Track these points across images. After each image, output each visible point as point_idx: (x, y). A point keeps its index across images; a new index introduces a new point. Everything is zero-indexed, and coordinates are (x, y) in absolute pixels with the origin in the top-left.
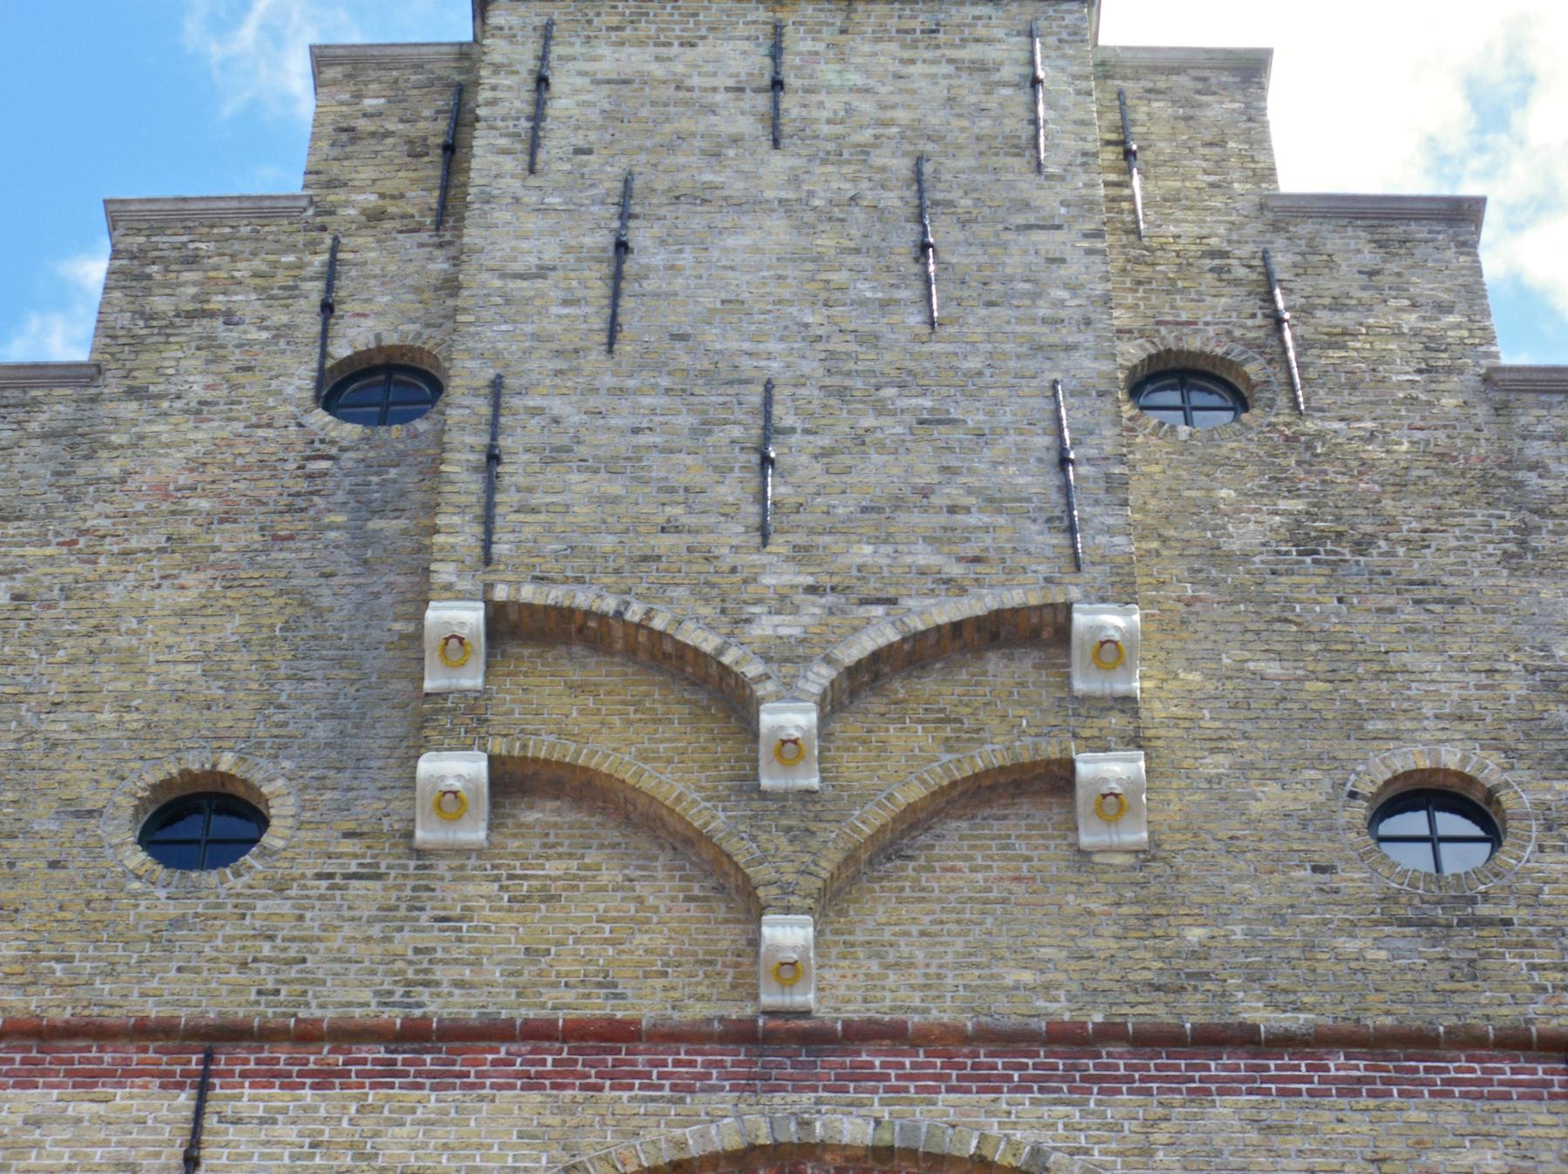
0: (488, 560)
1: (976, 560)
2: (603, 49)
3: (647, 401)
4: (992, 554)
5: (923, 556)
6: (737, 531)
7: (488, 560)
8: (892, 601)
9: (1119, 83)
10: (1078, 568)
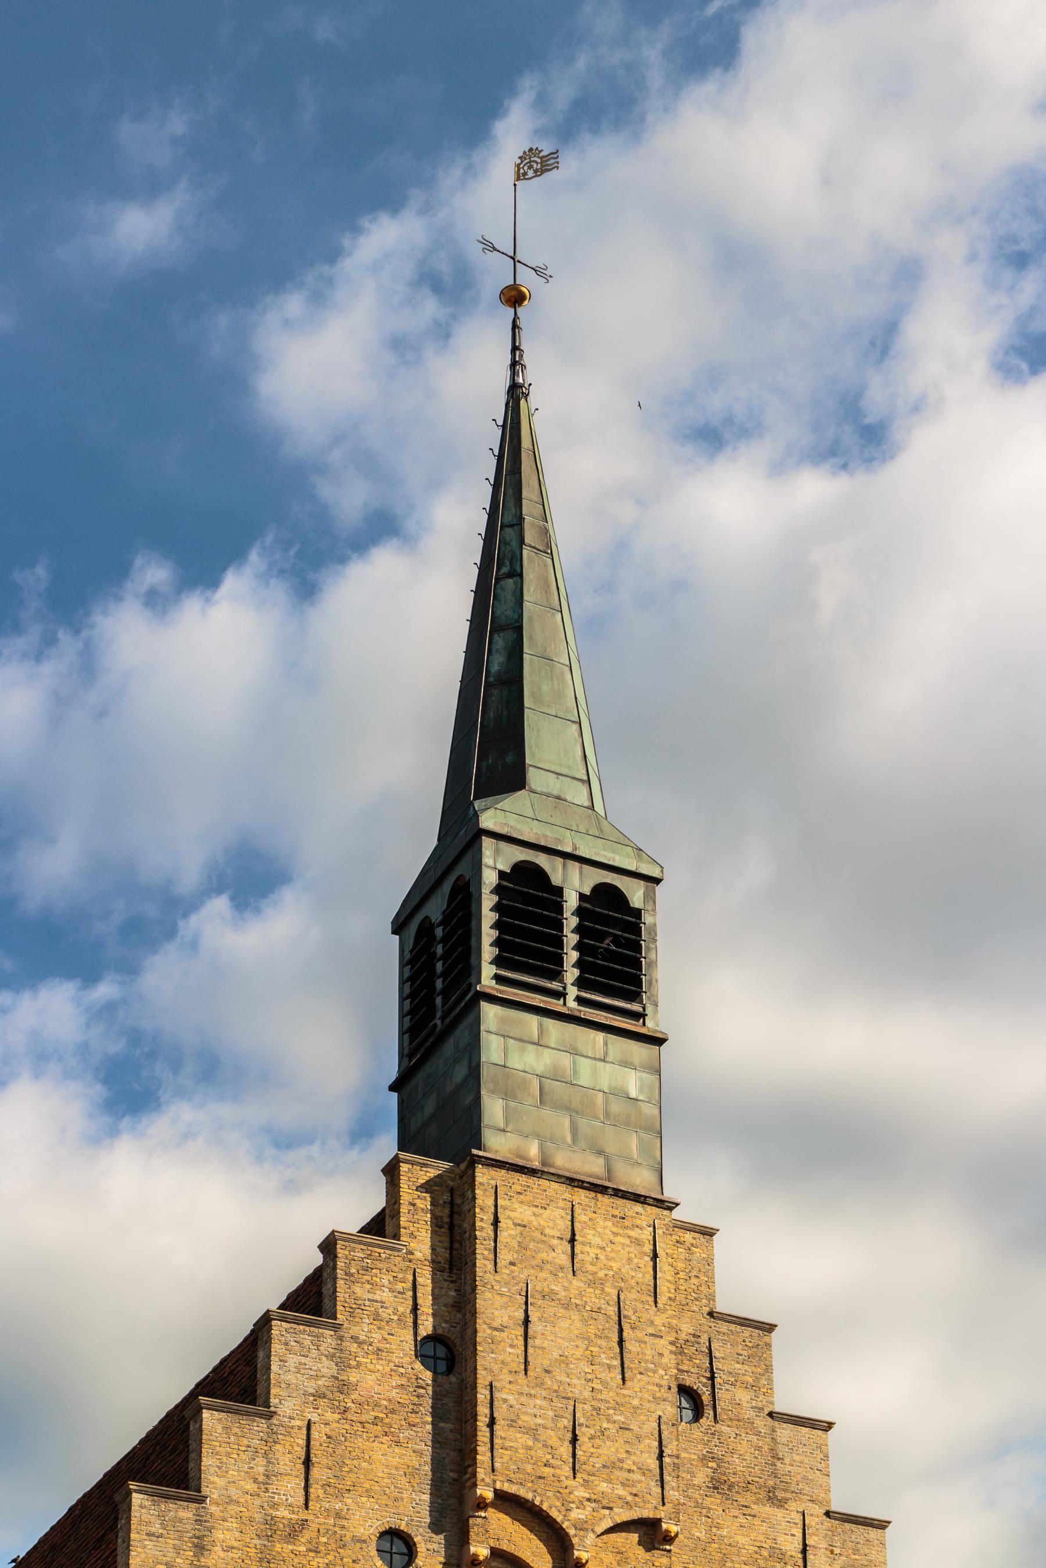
0: (493, 1471)
1: (636, 1495)
2: (516, 1205)
3: (538, 1402)
4: (640, 1494)
5: (621, 1491)
6: (567, 1470)
7: (493, 1471)
8: (611, 1509)
10: (664, 1504)
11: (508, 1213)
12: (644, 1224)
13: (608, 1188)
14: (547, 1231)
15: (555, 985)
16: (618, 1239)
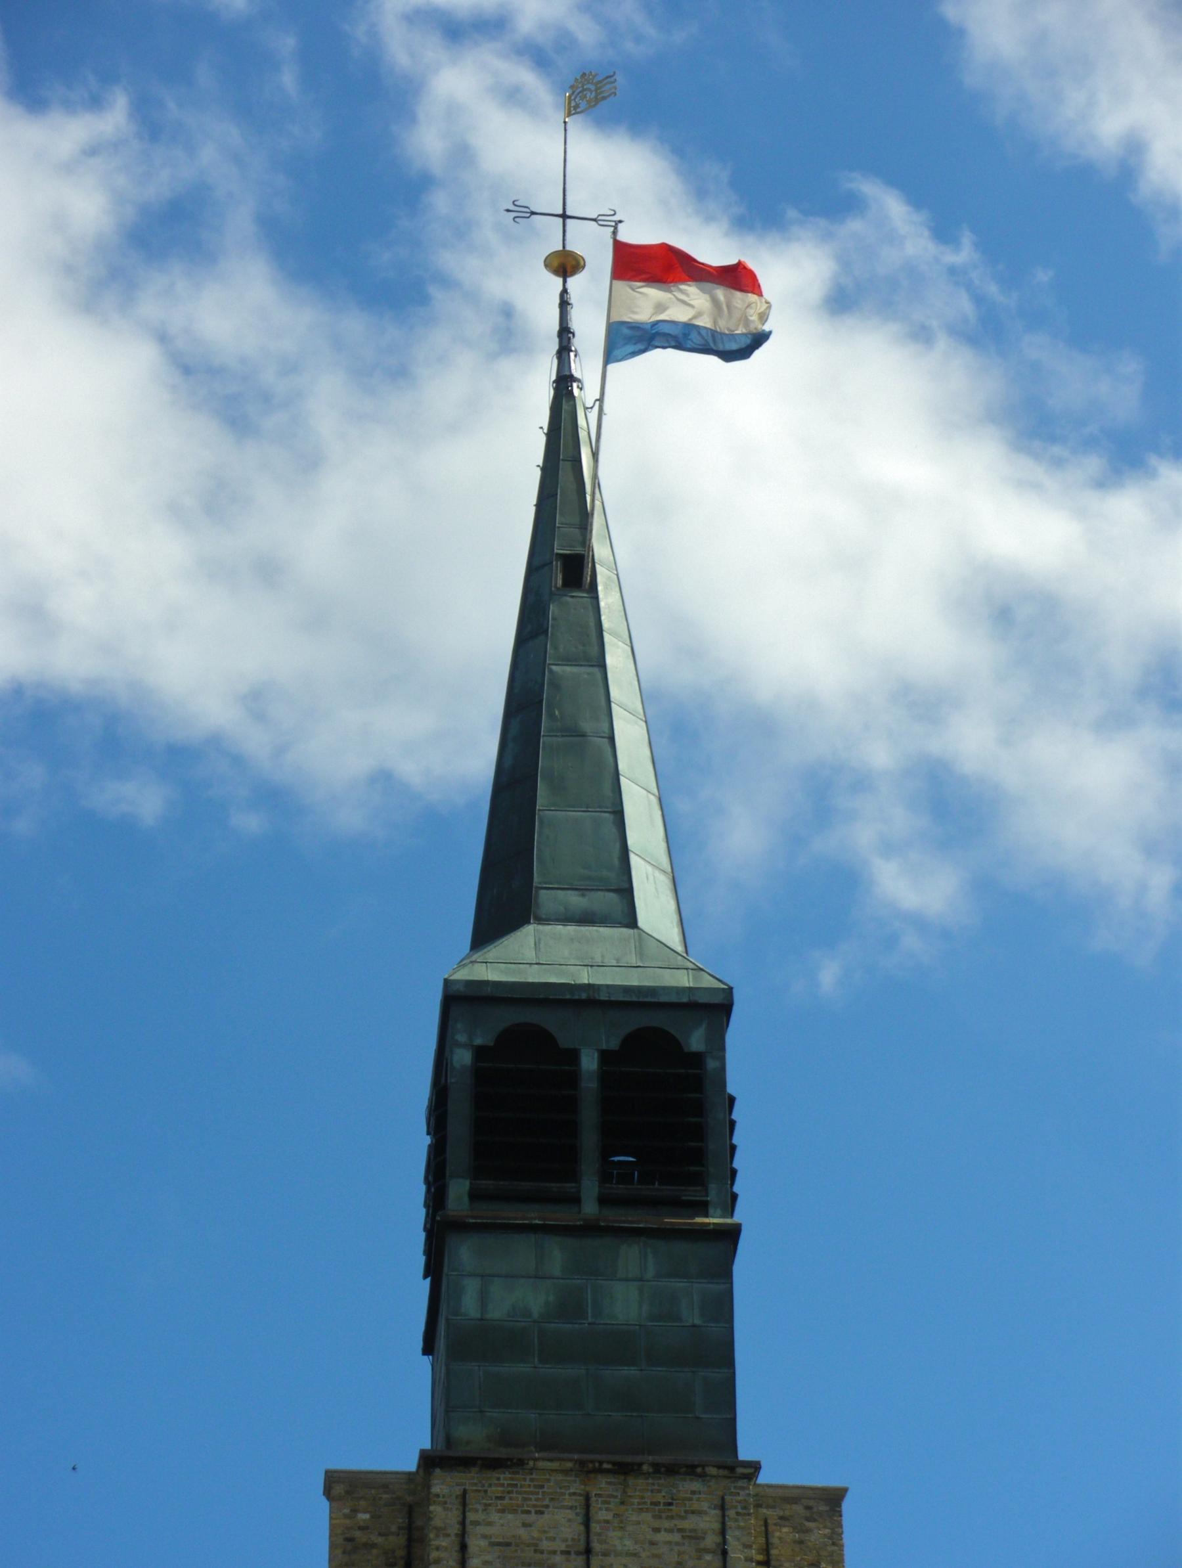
2: (495, 1517)
9: (765, 1511)
11: (481, 1530)
12: (705, 1506)
13: (640, 1465)
14: (545, 1545)
15: (569, 1187)
16: (662, 1537)
